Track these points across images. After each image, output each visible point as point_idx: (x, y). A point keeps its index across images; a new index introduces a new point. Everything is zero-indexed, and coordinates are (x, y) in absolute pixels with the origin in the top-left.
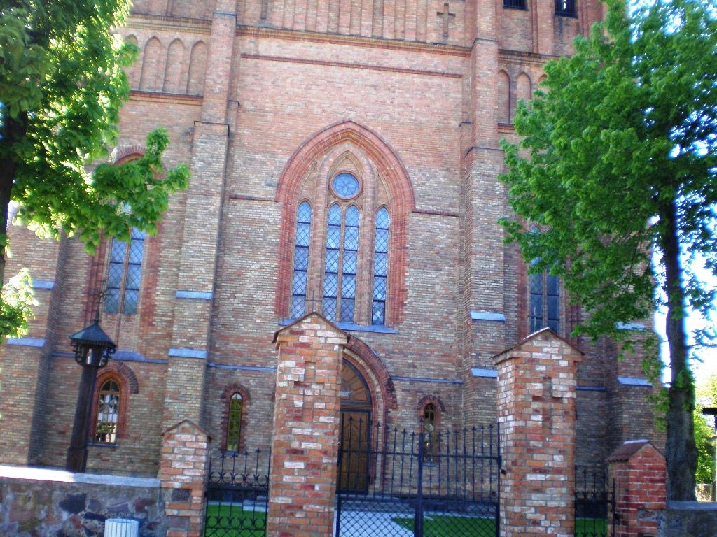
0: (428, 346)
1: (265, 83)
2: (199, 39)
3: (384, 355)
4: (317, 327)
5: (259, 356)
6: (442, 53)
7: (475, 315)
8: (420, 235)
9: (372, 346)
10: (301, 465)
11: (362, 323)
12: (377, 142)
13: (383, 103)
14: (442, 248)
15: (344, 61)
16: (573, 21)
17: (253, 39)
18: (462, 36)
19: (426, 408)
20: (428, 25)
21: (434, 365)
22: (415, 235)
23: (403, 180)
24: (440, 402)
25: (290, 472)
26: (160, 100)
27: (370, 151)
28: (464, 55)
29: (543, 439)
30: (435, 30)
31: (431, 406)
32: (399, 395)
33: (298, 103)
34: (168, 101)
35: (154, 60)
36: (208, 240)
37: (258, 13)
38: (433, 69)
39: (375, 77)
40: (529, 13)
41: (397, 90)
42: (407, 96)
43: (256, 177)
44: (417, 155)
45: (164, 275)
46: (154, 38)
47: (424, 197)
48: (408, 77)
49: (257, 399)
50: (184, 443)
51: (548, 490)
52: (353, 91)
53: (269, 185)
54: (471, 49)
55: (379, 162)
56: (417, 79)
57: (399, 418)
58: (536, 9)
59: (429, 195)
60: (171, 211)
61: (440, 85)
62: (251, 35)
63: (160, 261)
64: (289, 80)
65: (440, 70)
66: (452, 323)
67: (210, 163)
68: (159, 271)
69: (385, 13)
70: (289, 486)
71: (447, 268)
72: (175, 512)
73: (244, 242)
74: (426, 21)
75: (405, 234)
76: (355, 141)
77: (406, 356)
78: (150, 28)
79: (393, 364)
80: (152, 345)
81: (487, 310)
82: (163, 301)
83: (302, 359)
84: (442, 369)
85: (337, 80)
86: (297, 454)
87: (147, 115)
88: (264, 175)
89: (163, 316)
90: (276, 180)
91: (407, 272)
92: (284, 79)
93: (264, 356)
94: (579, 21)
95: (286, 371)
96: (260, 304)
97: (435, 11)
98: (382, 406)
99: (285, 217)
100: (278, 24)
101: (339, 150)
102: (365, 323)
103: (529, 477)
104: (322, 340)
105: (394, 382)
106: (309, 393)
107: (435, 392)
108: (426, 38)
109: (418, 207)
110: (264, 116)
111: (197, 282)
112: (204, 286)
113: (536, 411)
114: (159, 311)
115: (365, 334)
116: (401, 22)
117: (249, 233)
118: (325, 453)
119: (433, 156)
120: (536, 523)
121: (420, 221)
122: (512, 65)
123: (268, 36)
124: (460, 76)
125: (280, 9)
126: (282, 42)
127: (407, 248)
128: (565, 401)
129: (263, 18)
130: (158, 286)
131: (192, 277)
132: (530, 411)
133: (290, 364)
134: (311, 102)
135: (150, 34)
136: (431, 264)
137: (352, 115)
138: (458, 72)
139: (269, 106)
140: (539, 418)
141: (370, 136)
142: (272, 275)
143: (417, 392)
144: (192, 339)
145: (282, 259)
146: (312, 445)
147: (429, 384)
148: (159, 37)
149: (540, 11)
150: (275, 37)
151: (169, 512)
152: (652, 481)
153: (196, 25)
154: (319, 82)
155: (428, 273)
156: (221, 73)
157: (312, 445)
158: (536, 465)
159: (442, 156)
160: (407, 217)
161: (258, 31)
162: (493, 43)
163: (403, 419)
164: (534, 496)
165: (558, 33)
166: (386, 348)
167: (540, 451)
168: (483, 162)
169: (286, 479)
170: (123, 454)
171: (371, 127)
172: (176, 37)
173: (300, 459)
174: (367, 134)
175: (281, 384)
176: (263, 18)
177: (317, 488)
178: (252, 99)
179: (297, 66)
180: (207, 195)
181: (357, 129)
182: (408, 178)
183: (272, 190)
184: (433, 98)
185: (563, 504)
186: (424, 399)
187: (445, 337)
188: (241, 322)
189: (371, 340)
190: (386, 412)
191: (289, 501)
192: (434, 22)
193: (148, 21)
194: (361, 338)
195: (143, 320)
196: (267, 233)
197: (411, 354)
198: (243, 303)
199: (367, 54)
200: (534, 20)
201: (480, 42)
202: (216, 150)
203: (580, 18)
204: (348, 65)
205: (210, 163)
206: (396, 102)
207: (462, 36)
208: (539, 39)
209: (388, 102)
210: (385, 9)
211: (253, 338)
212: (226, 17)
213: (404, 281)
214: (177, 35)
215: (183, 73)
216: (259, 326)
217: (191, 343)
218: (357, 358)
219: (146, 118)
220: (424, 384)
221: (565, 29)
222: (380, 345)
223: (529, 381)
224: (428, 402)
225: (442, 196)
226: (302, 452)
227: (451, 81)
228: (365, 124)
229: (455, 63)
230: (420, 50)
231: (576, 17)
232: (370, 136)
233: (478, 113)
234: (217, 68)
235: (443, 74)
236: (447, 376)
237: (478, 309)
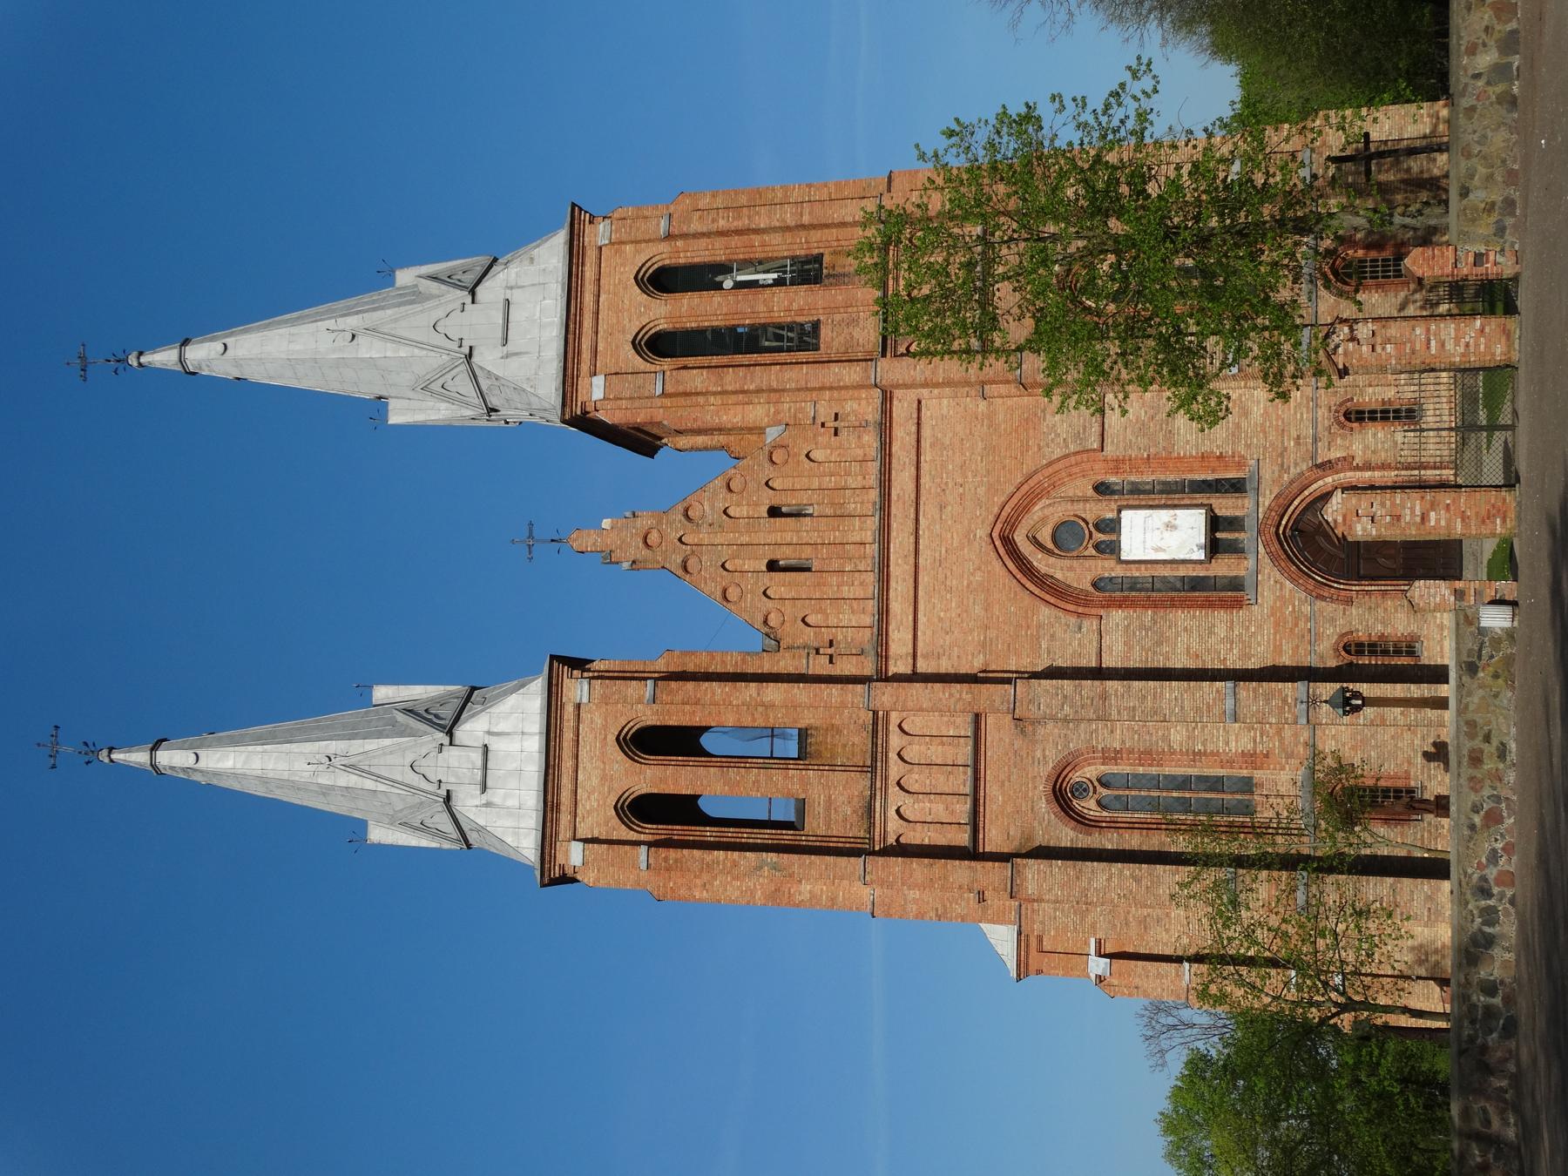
0: (1271, 423)
1: (947, 643)
3: (1286, 475)
4: (1330, 510)
5: (1296, 625)
8: (1131, 441)
9: (1276, 492)
10: (1432, 514)
11: (1246, 505)
12: (1015, 500)
13: (961, 496)
14: (1146, 412)
15: (912, 548)
16: (826, 259)
17: (891, 662)
18: (864, 403)
19: (1349, 419)
21: (1295, 413)
22: (1131, 447)
23: (1061, 465)
24: (1341, 405)
25: (1438, 521)
27: (1024, 508)
29: (1405, 343)
31: (1347, 415)
32: (1335, 454)
33: (971, 600)
36: (1161, 693)
39: (928, 509)
41: (945, 481)
42: (950, 467)
43: (1070, 644)
44: (1027, 451)
45: (1204, 744)
47: (1081, 439)
48: (924, 467)
49: (1351, 623)
50: (1421, 596)
51: (1443, 338)
52: (949, 536)
53: (1080, 628)
54: (884, 392)
55: (1039, 497)
56: (926, 457)
57: (1364, 453)
59: (1079, 432)
60: (1123, 742)
61: (933, 427)
63: (1187, 750)
64: (942, 614)
65: (914, 429)
66: (1241, 395)
67: (1065, 697)
70: (1448, 522)
72: (1472, 598)
73: (1155, 653)
75: (1130, 460)
76: (1013, 528)
77: (1285, 449)
79: (1296, 464)
80: (1293, 752)
82: (1237, 742)
83: (1355, 519)
84: (1300, 404)
85: (937, 555)
86: (1424, 518)
87: (1003, 782)
88: (1067, 636)
89: (1255, 741)
90: (1073, 620)
91: (1179, 454)
92: (940, 619)
93: (1297, 619)
94: (826, 252)
95: (1364, 530)
96: (1232, 628)
97: (833, 438)
98: (1349, 474)
99: (1120, 607)
101: (1025, 548)
102: (1246, 501)
103: (1433, 352)
104: (1340, 506)
106: (1379, 513)
107: (1330, 411)
109: (1095, 446)
110: (991, 640)
111: (1214, 699)
112: (1218, 691)
113: (1383, 349)
114: (1250, 747)
115: (1260, 499)
117: (1143, 648)
118: (1423, 498)
119: (1027, 430)
120: (1467, 345)
121: (1113, 442)
127: (1148, 455)
128: (1375, 328)
130: (1218, 751)
131: (1208, 707)
132: (1383, 353)
133: (1359, 528)
134: (968, 586)
135: (893, 790)
136: (1167, 424)
137: (982, 533)
139: (977, 636)
140: (1388, 346)
141: (1008, 509)
142: (1194, 617)
143: (1330, 433)
144: (1285, 701)
145: (1173, 606)
146: (1418, 508)
147: (1320, 419)
151: (1472, 603)
152: (1433, 258)
154: (941, 577)
155: (1179, 429)
156: (947, 695)
157: (1418, 508)
158: (1424, 347)
159: (1027, 420)
160: (1109, 458)
163: (1366, 447)
164: (1448, 347)
165: (846, 280)
166: (1276, 474)
167: (1413, 343)
169: (1443, 523)
170: (1429, 776)
171: (996, 510)
173: (1428, 515)
174: (1004, 514)
175: (1374, 533)
177: (1448, 502)
178: (970, 657)
179: (921, 607)
180: (1104, 697)
181: (999, 526)
182: (1059, 460)
183: (1086, 623)
184: (951, 435)
185: (1453, 326)
186: (1339, 423)
187: (1259, 402)
188: (1256, 649)
189: (1268, 492)
190: (1358, 468)
191: (1459, 520)
194: (1267, 504)
195: (1261, 768)
196: (1142, 627)
197: (1283, 443)
198: (1231, 649)
199: (901, 520)
201: (878, 380)
202: (1048, 691)
203: (821, 251)
204: (917, 543)
205: (1065, 697)
206: (960, 480)
207: (864, 403)
209: (961, 490)
211: (1275, 634)
213: (1191, 456)
214: (893, 756)
215: (943, 744)
216: (1260, 627)
218: (1292, 508)
219: (1007, 783)
220: (1319, 425)
221: (839, 270)
222: (1274, 481)
223: (1361, 356)
224: (1342, 419)
225: (1079, 417)
226: (1423, 514)
228: (991, 518)
231: (822, 255)
232: (1008, 509)
234: (940, 700)
236: (1307, 397)
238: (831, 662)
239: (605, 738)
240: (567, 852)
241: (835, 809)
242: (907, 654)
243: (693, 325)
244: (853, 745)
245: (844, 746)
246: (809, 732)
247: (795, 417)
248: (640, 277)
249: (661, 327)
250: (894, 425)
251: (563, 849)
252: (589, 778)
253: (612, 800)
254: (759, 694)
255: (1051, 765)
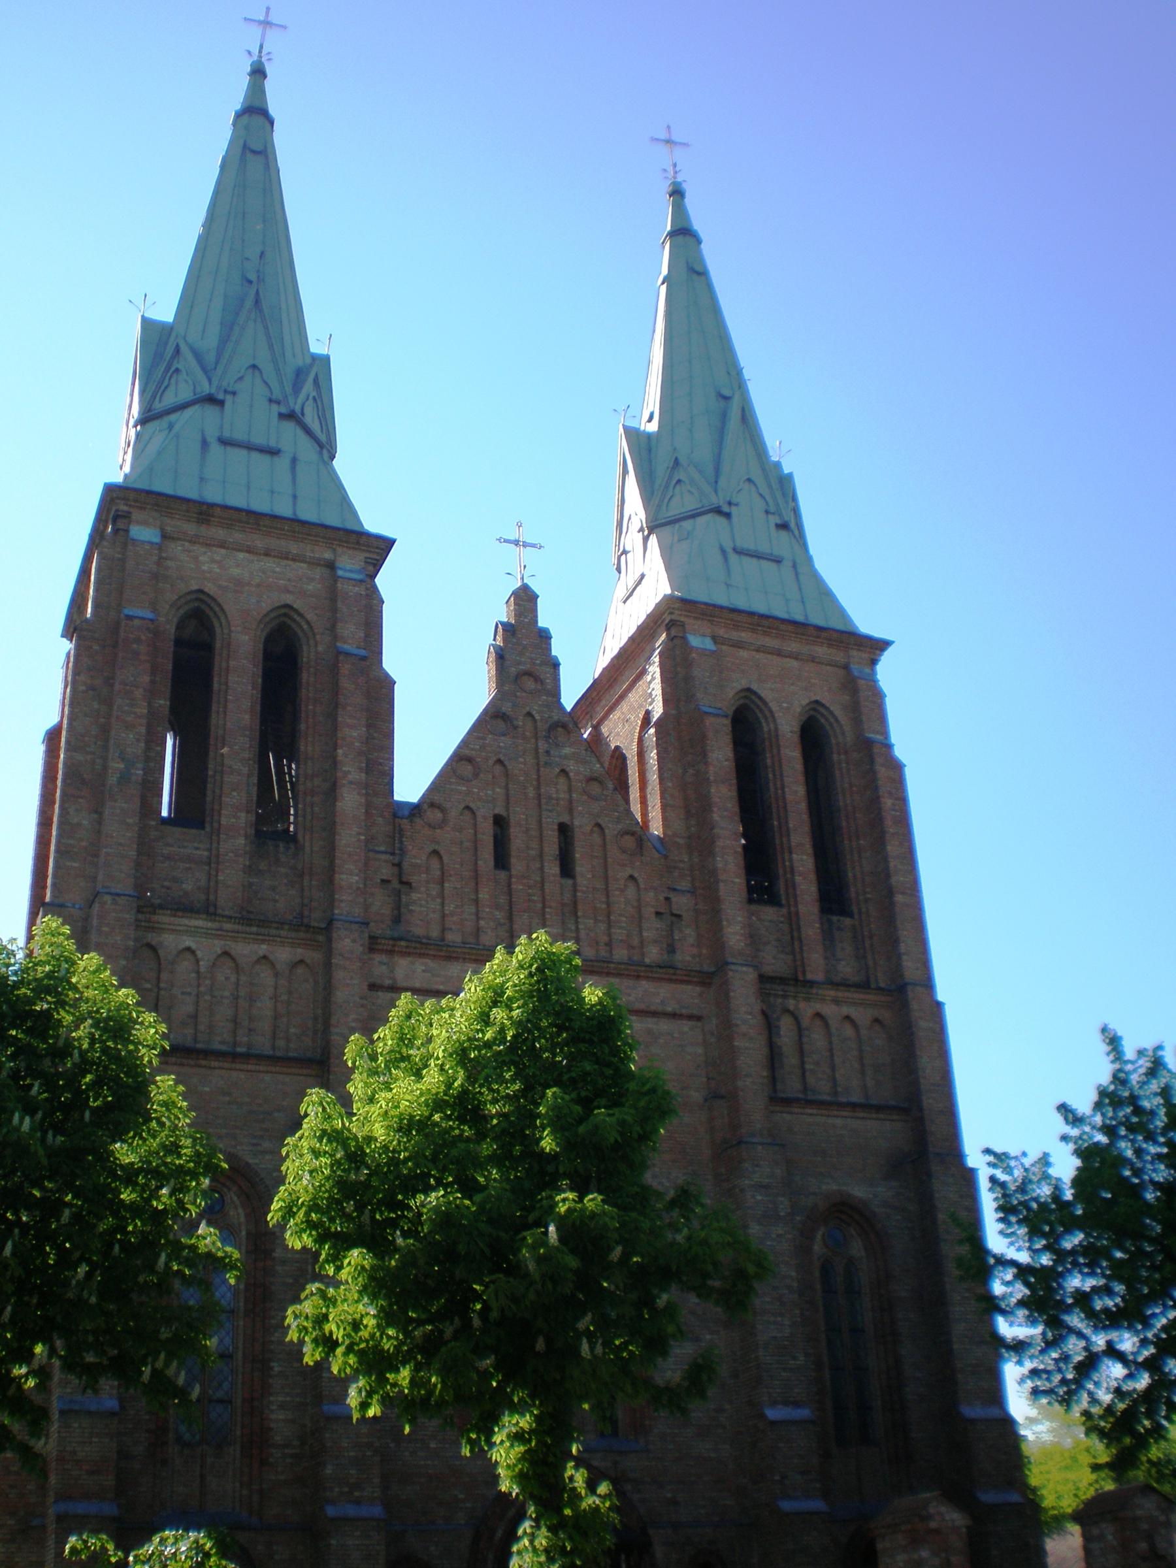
2: (298, 958)
6: (670, 980)
7: (772, 1414)
16: (848, 921)
17: (384, 958)
18: (695, 951)
20: (645, 934)
26: (250, 1067)
28: (702, 984)
30: (655, 942)
34: (261, 1068)
35: (227, 994)
37: (387, 911)
38: (660, 1008)
40: (784, 911)
46: (226, 954)
58: (796, 905)
62: (382, 951)
65: (669, 1009)
68: (272, 1368)
69: (580, 914)
71: (708, 1337)
74: (640, 927)
78: (218, 937)
81: (786, 1403)
97: (653, 910)
100: (419, 931)
105: (651, 1532)
108: (643, 955)
114: (278, 1439)
116: (603, 927)
122: (772, 999)
123: (409, 954)
124: (699, 1018)
125: (421, 906)
126: (431, 963)
129: (397, 920)
135: (218, 946)
138: (695, 1012)
148: (233, 953)
149: (802, 909)
150: (421, 955)
153: (294, 935)
156: (353, 1024)
161: (394, 946)
162: (751, 970)
168: (757, 1166)
172: (261, 953)
176: (397, 920)
192: (652, 928)
193: (216, 925)
200: (793, 921)
201: (733, 967)
203: (856, 917)
207: (695, 951)
208: (805, 955)
210: (580, 907)
212: (354, 926)
214: (263, 949)
217: (357, 1494)
219: (227, 1098)
227: (686, 1026)
229: (689, 996)
230: (638, 977)
231: (851, 915)
233: (740, 1084)
235: (674, 1016)
237: (774, 1403)
238: (383, 881)
239: (288, 592)
240: (145, 523)
241: (190, 868)
242: (394, 979)
243: (769, 761)
244: (276, 901)
245: (273, 888)
246: (292, 846)
247: (675, 868)
248: (202, 596)
249: (764, 724)
250: (673, 986)
251: (151, 520)
252: (238, 566)
253: (210, 588)
254: (351, 783)
255: (251, 1161)
